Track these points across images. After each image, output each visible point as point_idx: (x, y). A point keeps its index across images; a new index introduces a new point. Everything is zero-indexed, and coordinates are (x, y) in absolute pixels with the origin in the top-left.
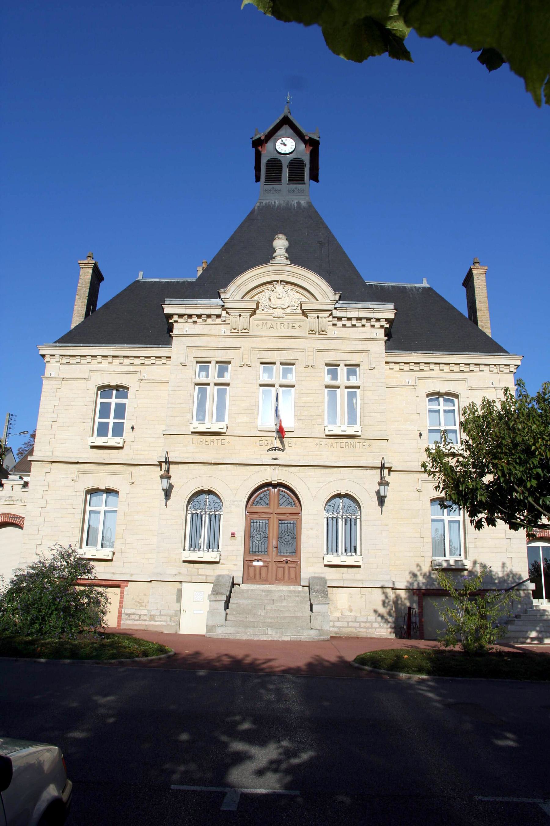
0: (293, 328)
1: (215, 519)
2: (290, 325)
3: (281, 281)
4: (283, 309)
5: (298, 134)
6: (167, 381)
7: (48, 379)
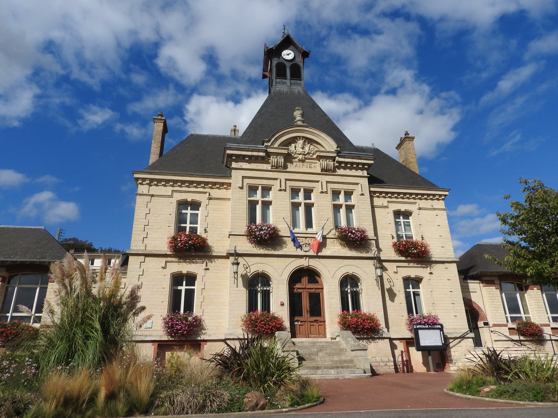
0: (310, 167)
1: (266, 295)
2: (308, 166)
3: (303, 137)
4: (303, 155)
5: (296, 48)
6: (229, 199)
7: (141, 195)
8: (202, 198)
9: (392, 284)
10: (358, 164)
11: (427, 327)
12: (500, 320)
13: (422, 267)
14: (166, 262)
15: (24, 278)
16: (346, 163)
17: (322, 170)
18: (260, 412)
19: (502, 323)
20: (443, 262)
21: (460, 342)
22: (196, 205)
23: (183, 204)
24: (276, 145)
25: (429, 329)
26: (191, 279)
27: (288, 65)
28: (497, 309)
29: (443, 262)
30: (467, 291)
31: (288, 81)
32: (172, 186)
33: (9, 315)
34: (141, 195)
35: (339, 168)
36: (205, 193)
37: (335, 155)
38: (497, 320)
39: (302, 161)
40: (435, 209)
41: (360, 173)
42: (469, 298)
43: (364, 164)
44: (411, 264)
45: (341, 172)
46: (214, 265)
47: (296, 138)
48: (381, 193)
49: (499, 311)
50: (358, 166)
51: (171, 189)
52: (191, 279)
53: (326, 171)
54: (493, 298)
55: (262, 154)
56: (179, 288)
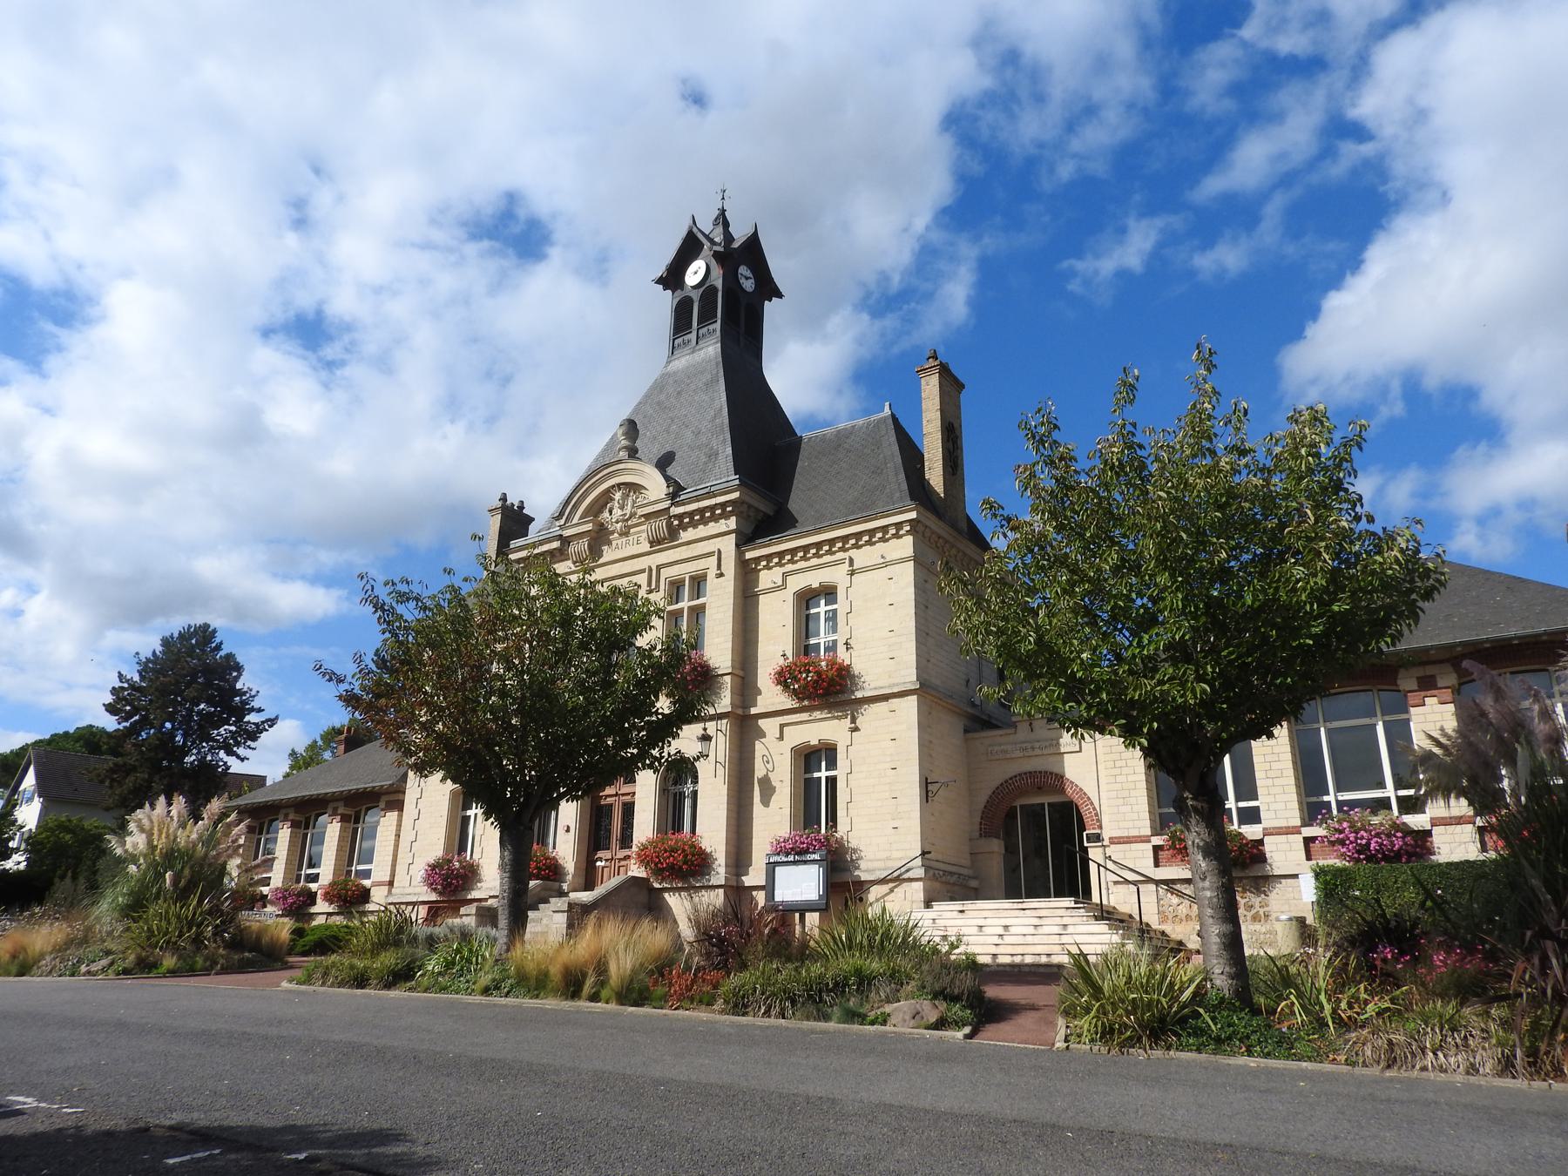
8: (836, 575)
9: (770, 766)
10: (712, 508)
11: (791, 858)
12: (1130, 824)
13: (834, 718)
14: (782, 726)
15: (1343, 702)
16: (691, 514)
17: (652, 543)
18: (479, 999)
19: (1283, 823)
20: (885, 698)
21: (892, 891)
22: (829, 592)
23: (806, 599)
24: (575, 521)
25: (794, 863)
26: (826, 753)
27: (696, 295)
28: (1126, 794)
29: (885, 698)
30: (1052, 751)
31: (693, 336)
32: (780, 564)
33: (1330, 798)
34: (903, 560)
35: (685, 529)
36: (841, 562)
37: (666, 504)
38: (1122, 825)
39: (625, 533)
40: (886, 565)
41: (713, 528)
42: (1055, 770)
43: (723, 505)
44: (817, 714)
45: (689, 534)
46: (871, 716)
47: (608, 491)
48: (769, 557)
49: (1132, 800)
50: (692, 519)
51: (778, 571)
52: (826, 753)
53: (659, 543)
54: (1118, 764)
55: (556, 544)
56: (816, 775)
